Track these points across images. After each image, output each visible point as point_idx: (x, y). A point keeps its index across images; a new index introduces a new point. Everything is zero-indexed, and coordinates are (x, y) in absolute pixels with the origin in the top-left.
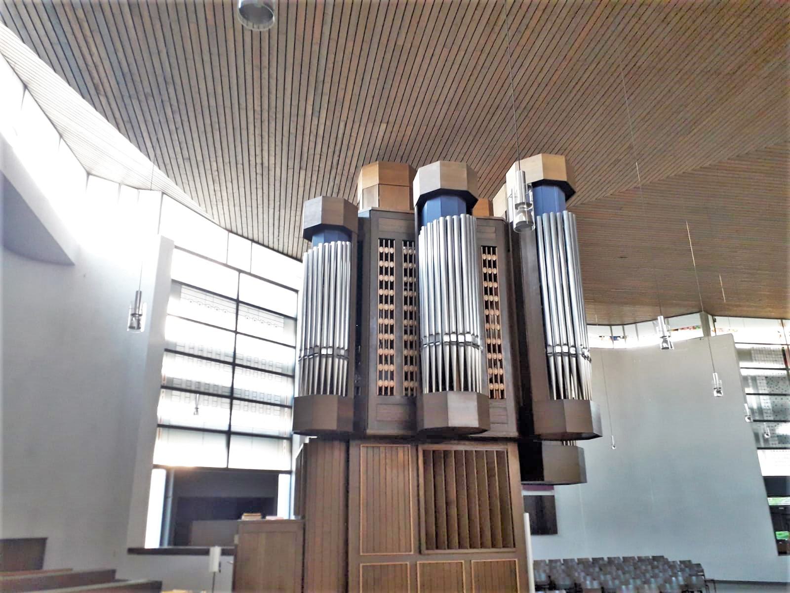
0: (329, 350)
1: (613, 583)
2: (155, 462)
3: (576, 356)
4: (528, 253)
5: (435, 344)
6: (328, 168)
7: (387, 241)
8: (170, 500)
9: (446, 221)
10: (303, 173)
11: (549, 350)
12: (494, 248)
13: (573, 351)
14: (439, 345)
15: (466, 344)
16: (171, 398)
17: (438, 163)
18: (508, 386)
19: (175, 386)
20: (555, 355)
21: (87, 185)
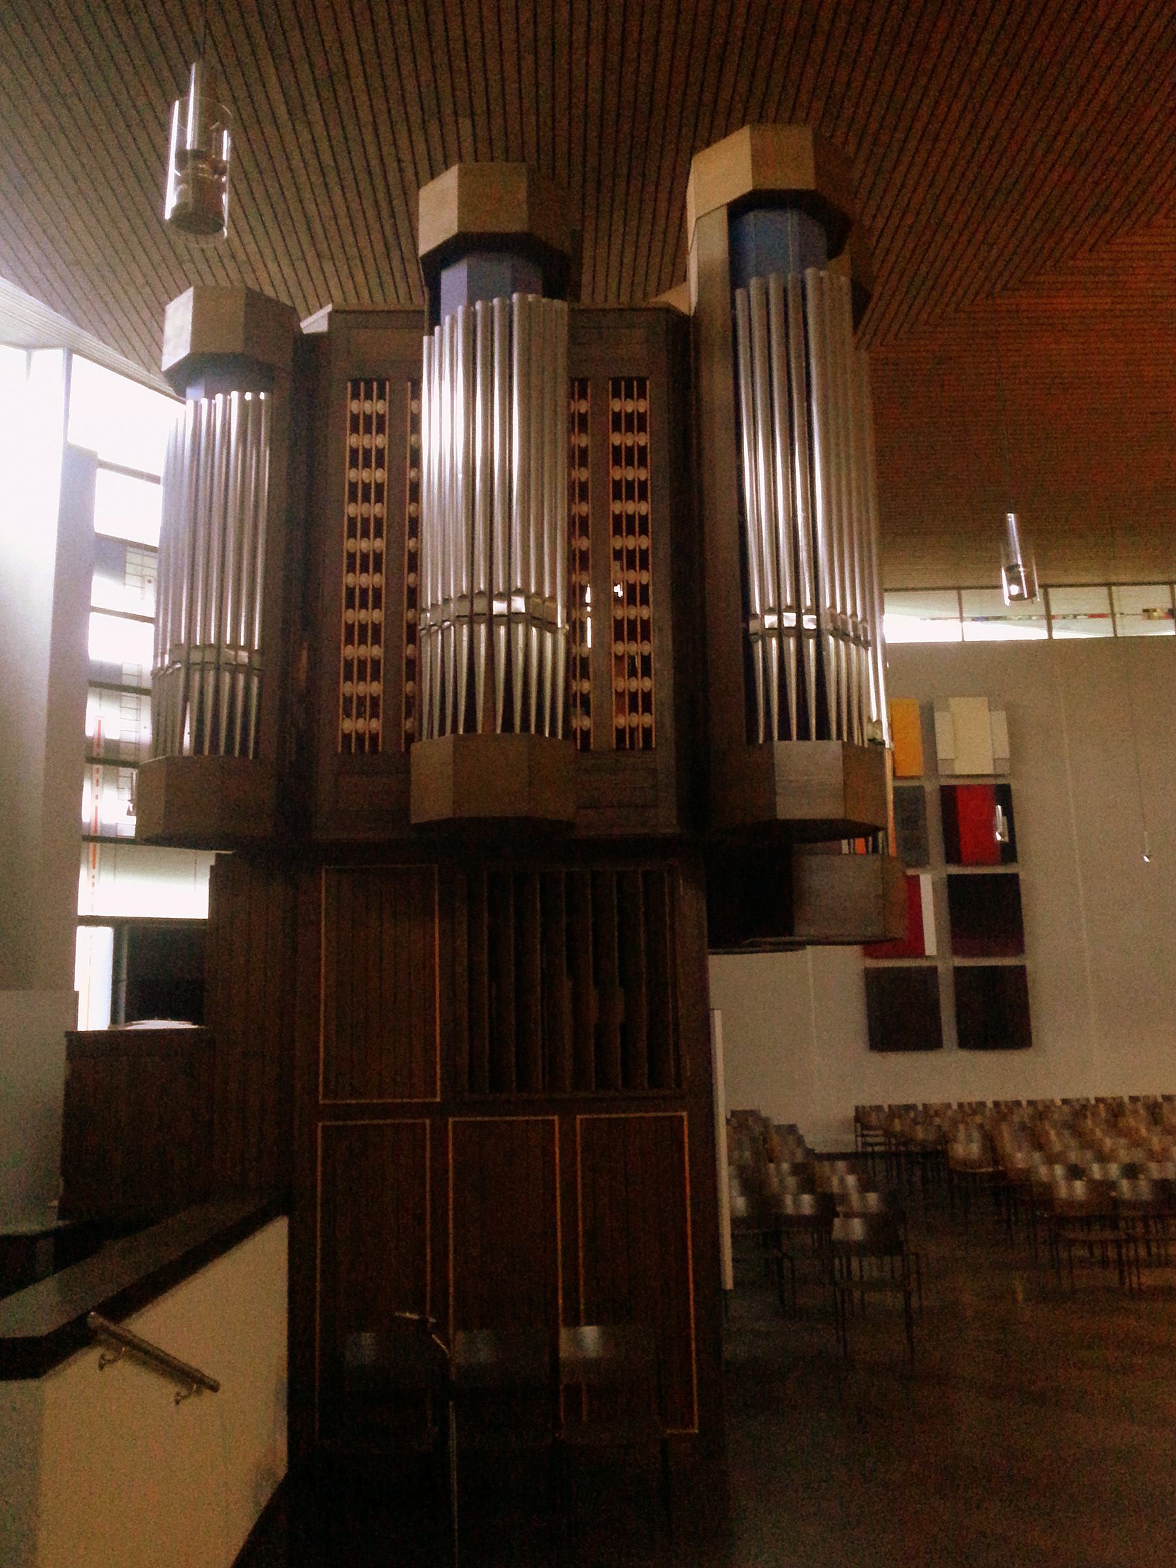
0: (208, 652)
1: (863, 1199)
2: (83, 910)
3: (818, 634)
4: (715, 383)
5: (440, 627)
6: (380, 248)
7: (369, 383)
8: (123, 987)
9: (475, 314)
10: (328, 267)
11: (754, 626)
12: (642, 382)
13: (809, 623)
14: (449, 627)
15: (511, 618)
16: (117, 781)
17: (454, 170)
18: (660, 724)
19: (123, 757)
20: (766, 634)
21: (29, 364)
